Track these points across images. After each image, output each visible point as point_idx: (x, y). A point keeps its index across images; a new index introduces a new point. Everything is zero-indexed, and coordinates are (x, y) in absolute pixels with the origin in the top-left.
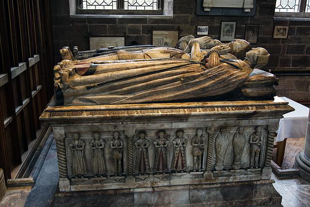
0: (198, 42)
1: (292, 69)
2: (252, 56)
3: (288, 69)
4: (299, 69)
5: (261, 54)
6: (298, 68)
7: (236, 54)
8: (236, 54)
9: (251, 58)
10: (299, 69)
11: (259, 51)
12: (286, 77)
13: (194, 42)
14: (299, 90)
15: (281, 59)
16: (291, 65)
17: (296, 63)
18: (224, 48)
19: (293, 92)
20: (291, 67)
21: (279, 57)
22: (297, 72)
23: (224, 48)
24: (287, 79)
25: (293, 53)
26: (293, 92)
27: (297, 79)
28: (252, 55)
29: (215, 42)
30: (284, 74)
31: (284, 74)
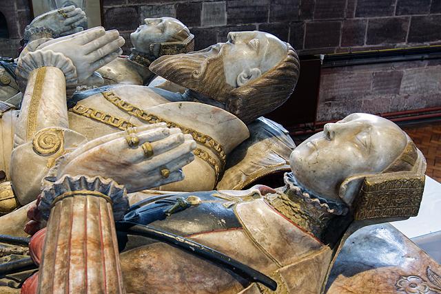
0: (55, 61)
1: (367, 49)
2: (325, 178)
3: (358, 50)
4: (382, 48)
5: (380, 162)
6: (381, 46)
7: (239, 103)
8: (239, 103)
9: (324, 187)
10: (382, 48)
11: (368, 148)
12: (355, 67)
13: (35, 65)
14: (382, 93)
15: (344, 30)
16: (365, 41)
17: (379, 33)
18: (149, 155)
19: (369, 98)
20: (365, 46)
21: (339, 24)
22: (378, 55)
23: (149, 155)
24: (358, 72)
25: (370, 14)
26: (369, 98)
27: (376, 69)
28: (324, 170)
29: (163, 29)
30: (351, 62)
31: (351, 62)
